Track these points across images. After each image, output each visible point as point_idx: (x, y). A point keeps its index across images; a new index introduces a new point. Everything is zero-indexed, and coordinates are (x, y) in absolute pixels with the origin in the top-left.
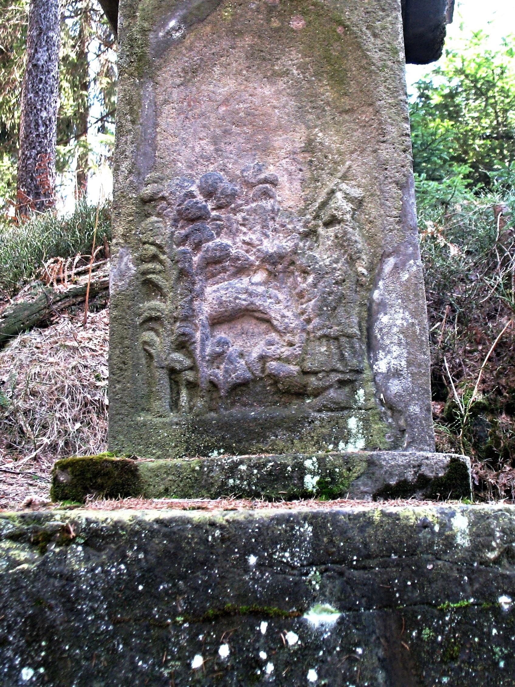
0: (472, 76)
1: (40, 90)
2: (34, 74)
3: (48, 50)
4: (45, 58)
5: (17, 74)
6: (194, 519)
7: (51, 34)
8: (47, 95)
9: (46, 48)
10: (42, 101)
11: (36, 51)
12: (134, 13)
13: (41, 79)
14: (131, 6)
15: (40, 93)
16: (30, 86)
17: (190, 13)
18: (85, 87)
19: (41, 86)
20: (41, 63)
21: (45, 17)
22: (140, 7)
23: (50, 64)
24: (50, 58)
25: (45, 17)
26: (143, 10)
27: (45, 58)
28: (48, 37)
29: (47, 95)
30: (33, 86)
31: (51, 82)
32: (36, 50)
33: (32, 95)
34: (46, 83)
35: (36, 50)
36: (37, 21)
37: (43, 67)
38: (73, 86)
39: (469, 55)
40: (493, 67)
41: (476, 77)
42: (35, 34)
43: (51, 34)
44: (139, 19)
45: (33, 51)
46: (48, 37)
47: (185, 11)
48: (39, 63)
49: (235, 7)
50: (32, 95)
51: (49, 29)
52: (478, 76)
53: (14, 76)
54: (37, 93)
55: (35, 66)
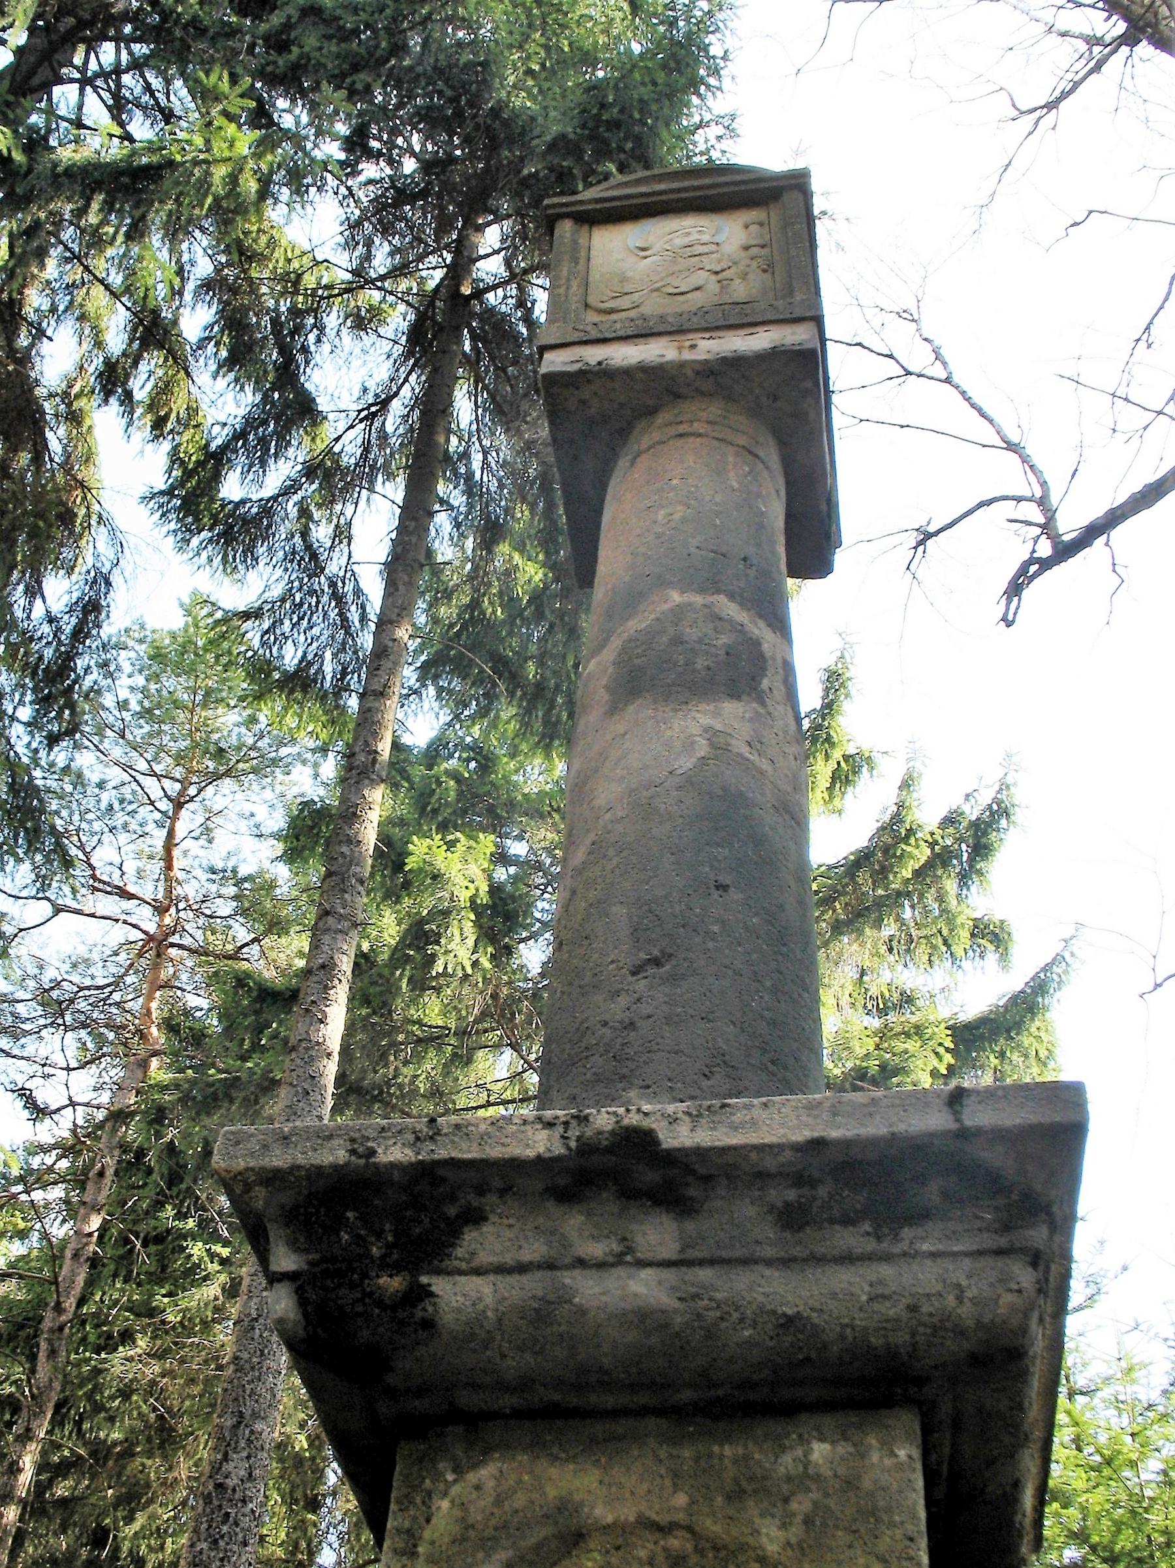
0: (1105, 1548)
1: (222, 1537)
2: (216, 1503)
3: (248, 1457)
4: (242, 1473)
5: (184, 1469)
6: (614, 1207)
7: (259, 1426)
8: (235, 1548)
9: (245, 1454)
10: (222, 1560)
11: (226, 1458)
12: (415, 1546)
13: (227, 1515)
14: (409, 1532)
15: (222, 1543)
16: (205, 1526)
17: (522, 1558)
18: (314, 1505)
19: (225, 1529)
20: (230, 1483)
21: (253, 1392)
22: (427, 1534)
23: (248, 1485)
24: (250, 1475)
25: (253, 1392)
26: (433, 1543)
27: (242, 1473)
28: (252, 1432)
29: (235, 1548)
30: (210, 1526)
31: (245, 1522)
32: (226, 1455)
33: (204, 1545)
34: (236, 1524)
35: (226, 1455)
36: (236, 1399)
37: (234, 1490)
38: (290, 1500)
39: (1096, 1499)
40: (1147, 1529)
41: (1112, 1551)
42: (229, 1423)
43: (259, 1426)
44: (422, 1559)
45: (219, 1457)
46: (252, 1432)
47: (511, 1553)
48: (228, 1481)
49: (608, 1552)
50: (204, 1545)
51: (255, 1416)
52: (1118, 1548)
53: (176, 1474)
54: (216, 1542)
55: (220, 1486)
